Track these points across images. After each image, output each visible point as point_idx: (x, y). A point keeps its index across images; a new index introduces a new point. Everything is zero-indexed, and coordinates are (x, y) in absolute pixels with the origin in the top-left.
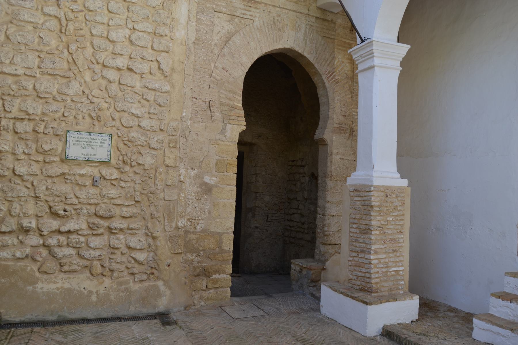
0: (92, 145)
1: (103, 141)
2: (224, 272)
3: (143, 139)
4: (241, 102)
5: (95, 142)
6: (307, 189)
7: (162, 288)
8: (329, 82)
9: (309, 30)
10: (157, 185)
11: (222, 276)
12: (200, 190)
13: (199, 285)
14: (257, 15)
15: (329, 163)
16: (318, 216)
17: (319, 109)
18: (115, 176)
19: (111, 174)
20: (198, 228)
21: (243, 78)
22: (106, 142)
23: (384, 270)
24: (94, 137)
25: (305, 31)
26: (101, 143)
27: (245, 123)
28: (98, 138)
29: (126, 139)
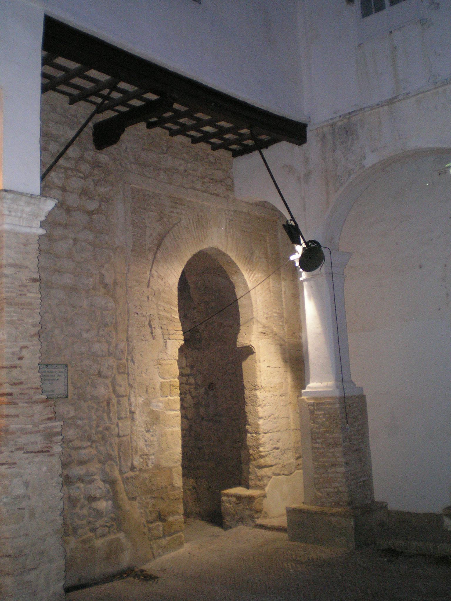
0: (50, 380)
1: (59, 374)
2: (177, 513)
3: (95, 366)
4: (178, 314)
5: (53, 376)
6: (203, 404)
7: (124, 541)
8: (250, 281)
9: (229, 224)
10: (111, 419)
11: (177, 517)
12: (148, 419)
13: (156, 532)
14: (183, 212)
15: (258, 373)
16: (249, 435)
17: (238, 312)
18: (72, 414)
19: (68, 412)
20: (151, 466)
21: (177, 285)
22: (63, 374)
23: (355, 481)
24: (51, 370)
25: (226, 226)
26: (59, 376)
27: (182, 337)
28: (54, 370)
29: (79, 369)
